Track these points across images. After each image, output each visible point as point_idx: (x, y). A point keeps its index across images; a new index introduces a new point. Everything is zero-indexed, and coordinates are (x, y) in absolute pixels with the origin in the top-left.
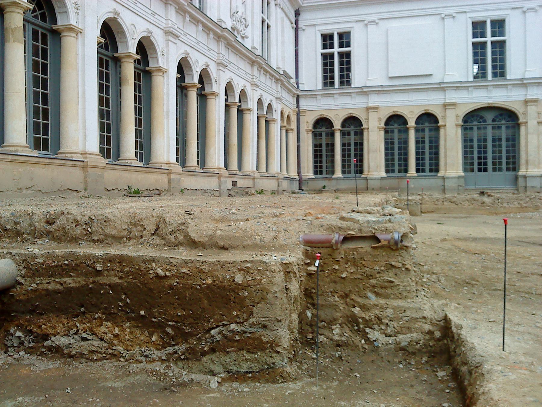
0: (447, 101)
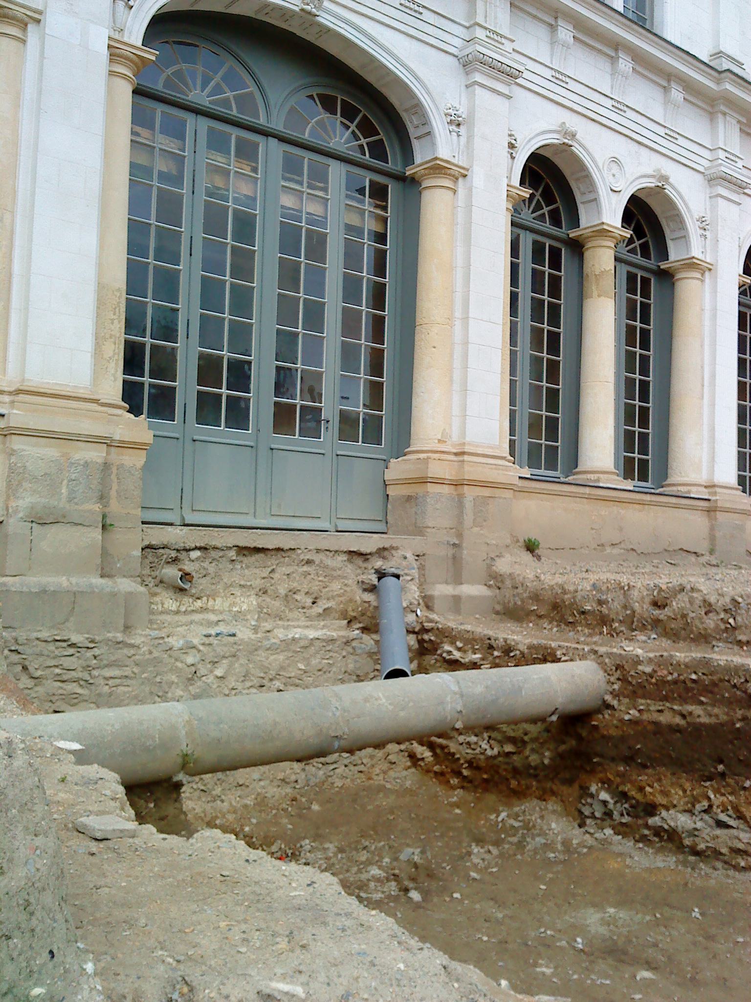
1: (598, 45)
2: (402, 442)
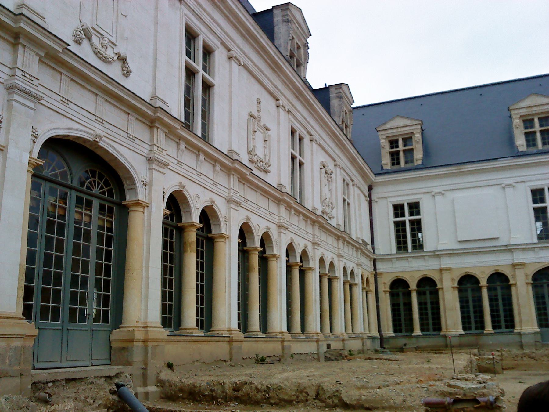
0: (515, 262)
1: (193, 150)
2: (118, 322)
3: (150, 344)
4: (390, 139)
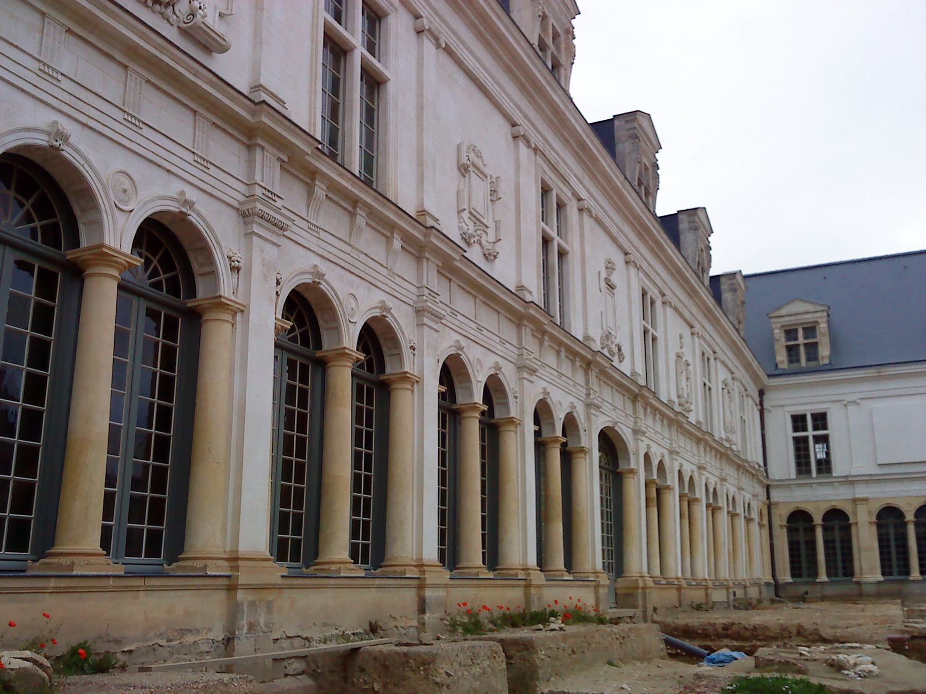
3: (648, 591)
4: (788, 328)
